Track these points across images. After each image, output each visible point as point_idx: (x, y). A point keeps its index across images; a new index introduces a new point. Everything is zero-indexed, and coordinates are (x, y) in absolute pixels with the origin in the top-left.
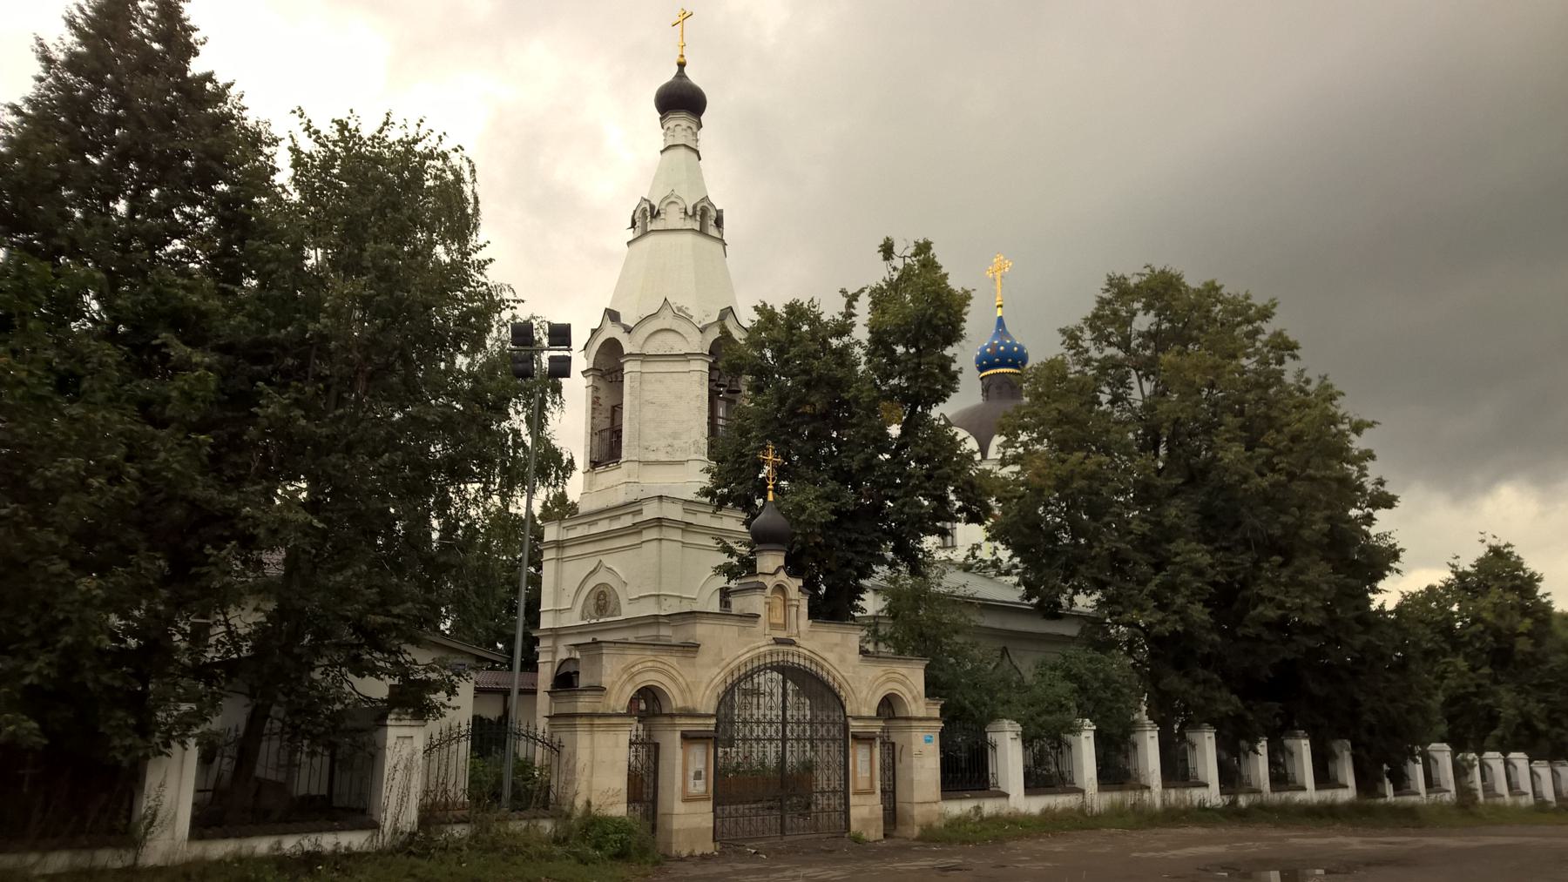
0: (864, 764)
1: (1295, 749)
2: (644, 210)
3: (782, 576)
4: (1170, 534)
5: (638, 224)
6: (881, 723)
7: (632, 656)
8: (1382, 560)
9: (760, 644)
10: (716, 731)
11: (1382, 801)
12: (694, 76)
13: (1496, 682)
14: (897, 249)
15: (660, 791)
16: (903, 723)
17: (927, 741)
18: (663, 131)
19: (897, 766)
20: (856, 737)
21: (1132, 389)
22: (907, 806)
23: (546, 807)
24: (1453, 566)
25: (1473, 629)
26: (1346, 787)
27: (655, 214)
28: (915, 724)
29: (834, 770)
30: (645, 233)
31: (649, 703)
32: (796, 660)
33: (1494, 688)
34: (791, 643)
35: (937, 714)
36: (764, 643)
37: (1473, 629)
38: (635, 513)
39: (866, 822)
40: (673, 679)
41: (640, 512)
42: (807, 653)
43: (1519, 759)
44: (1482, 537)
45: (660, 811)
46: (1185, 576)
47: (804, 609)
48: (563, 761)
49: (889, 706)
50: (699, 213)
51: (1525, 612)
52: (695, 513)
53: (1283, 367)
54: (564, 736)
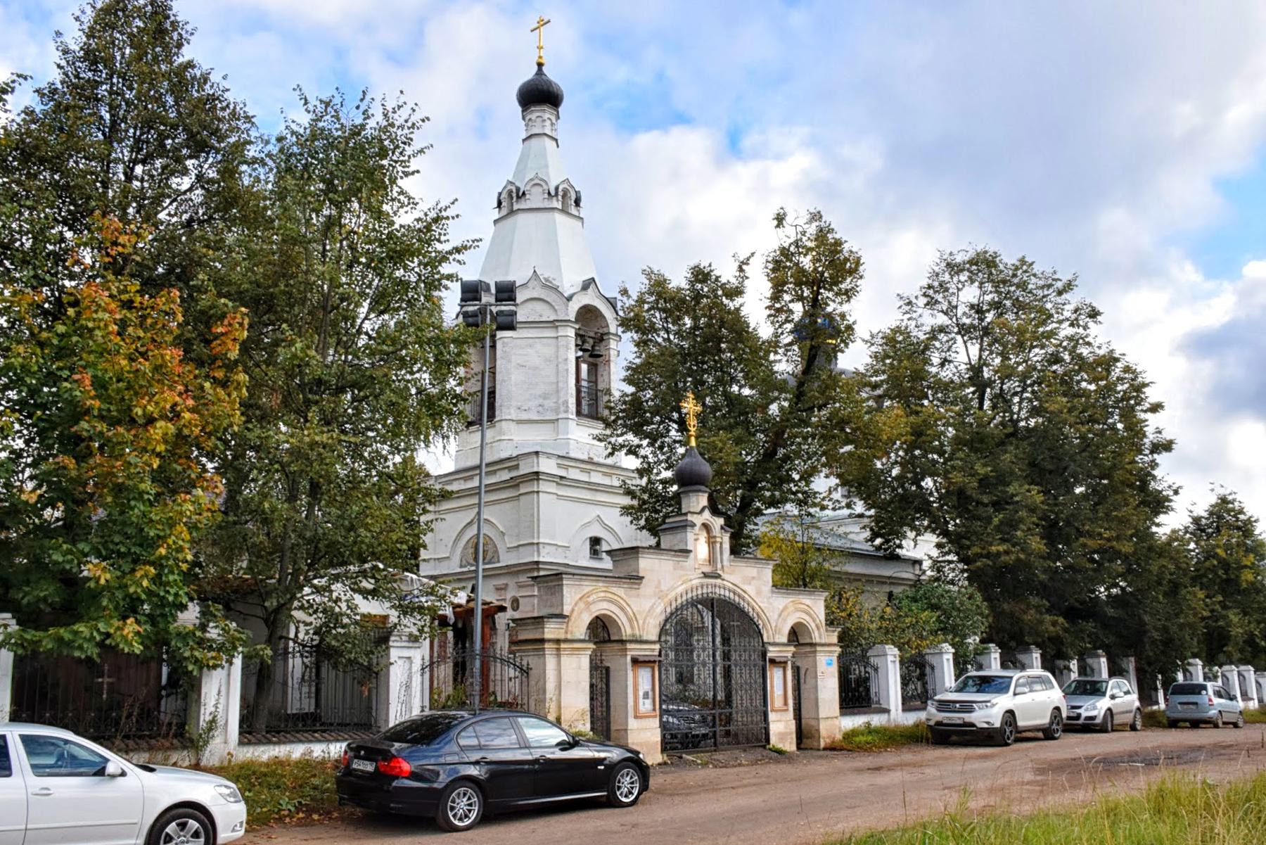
0: (778, 682)
1: (1095, 666)
2: (510, 192)
3: (707, 514)
4: (1002, 479)
5: (504, 204)
6: (792, 649)
7: (588, 586)
8: (1159, 504)
9: (692, 577)
10: (660, 655)
11: (1155, 708)
12: (551, 73)
13: (1225, 607)
14: (789, 219)
15: (612, 709)
16: (808, 649)
17: (829, 664)
18: (523, 123)
19: (802, 687)
20: (773, 661)
21: (957, 353)
22: (813, 723)
23: (609, 739)
24: (1191, 512)
25: (1207, 564)
26: (1253, 699)
27: (521, 195)
28: (819, 648)
29: (756, 691)
30: (512, 212)
31: (602, 630)
32: (722, 593)
33: (1224, 612)
34: (719, 576)
35: (835, 640)
36: (696, 576)
37: (1207, 564)
38: (510, 469)
39: (782, 736)
40: (622, 609)
41: (517, 467)
42: (731, 586)
43: (1249, 671)
44: (1212, 486)
45: (613, 727)
46: (1023, 513)
47: (727, 546)
48: (532, 683)
49: (796, 635)
50: (561, 193)
51: (1248, 550)
52: (566, 467)
53: (1088, 331)
54: (530, 660)
